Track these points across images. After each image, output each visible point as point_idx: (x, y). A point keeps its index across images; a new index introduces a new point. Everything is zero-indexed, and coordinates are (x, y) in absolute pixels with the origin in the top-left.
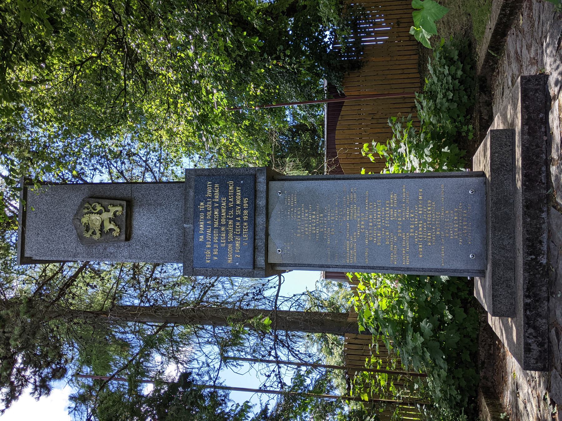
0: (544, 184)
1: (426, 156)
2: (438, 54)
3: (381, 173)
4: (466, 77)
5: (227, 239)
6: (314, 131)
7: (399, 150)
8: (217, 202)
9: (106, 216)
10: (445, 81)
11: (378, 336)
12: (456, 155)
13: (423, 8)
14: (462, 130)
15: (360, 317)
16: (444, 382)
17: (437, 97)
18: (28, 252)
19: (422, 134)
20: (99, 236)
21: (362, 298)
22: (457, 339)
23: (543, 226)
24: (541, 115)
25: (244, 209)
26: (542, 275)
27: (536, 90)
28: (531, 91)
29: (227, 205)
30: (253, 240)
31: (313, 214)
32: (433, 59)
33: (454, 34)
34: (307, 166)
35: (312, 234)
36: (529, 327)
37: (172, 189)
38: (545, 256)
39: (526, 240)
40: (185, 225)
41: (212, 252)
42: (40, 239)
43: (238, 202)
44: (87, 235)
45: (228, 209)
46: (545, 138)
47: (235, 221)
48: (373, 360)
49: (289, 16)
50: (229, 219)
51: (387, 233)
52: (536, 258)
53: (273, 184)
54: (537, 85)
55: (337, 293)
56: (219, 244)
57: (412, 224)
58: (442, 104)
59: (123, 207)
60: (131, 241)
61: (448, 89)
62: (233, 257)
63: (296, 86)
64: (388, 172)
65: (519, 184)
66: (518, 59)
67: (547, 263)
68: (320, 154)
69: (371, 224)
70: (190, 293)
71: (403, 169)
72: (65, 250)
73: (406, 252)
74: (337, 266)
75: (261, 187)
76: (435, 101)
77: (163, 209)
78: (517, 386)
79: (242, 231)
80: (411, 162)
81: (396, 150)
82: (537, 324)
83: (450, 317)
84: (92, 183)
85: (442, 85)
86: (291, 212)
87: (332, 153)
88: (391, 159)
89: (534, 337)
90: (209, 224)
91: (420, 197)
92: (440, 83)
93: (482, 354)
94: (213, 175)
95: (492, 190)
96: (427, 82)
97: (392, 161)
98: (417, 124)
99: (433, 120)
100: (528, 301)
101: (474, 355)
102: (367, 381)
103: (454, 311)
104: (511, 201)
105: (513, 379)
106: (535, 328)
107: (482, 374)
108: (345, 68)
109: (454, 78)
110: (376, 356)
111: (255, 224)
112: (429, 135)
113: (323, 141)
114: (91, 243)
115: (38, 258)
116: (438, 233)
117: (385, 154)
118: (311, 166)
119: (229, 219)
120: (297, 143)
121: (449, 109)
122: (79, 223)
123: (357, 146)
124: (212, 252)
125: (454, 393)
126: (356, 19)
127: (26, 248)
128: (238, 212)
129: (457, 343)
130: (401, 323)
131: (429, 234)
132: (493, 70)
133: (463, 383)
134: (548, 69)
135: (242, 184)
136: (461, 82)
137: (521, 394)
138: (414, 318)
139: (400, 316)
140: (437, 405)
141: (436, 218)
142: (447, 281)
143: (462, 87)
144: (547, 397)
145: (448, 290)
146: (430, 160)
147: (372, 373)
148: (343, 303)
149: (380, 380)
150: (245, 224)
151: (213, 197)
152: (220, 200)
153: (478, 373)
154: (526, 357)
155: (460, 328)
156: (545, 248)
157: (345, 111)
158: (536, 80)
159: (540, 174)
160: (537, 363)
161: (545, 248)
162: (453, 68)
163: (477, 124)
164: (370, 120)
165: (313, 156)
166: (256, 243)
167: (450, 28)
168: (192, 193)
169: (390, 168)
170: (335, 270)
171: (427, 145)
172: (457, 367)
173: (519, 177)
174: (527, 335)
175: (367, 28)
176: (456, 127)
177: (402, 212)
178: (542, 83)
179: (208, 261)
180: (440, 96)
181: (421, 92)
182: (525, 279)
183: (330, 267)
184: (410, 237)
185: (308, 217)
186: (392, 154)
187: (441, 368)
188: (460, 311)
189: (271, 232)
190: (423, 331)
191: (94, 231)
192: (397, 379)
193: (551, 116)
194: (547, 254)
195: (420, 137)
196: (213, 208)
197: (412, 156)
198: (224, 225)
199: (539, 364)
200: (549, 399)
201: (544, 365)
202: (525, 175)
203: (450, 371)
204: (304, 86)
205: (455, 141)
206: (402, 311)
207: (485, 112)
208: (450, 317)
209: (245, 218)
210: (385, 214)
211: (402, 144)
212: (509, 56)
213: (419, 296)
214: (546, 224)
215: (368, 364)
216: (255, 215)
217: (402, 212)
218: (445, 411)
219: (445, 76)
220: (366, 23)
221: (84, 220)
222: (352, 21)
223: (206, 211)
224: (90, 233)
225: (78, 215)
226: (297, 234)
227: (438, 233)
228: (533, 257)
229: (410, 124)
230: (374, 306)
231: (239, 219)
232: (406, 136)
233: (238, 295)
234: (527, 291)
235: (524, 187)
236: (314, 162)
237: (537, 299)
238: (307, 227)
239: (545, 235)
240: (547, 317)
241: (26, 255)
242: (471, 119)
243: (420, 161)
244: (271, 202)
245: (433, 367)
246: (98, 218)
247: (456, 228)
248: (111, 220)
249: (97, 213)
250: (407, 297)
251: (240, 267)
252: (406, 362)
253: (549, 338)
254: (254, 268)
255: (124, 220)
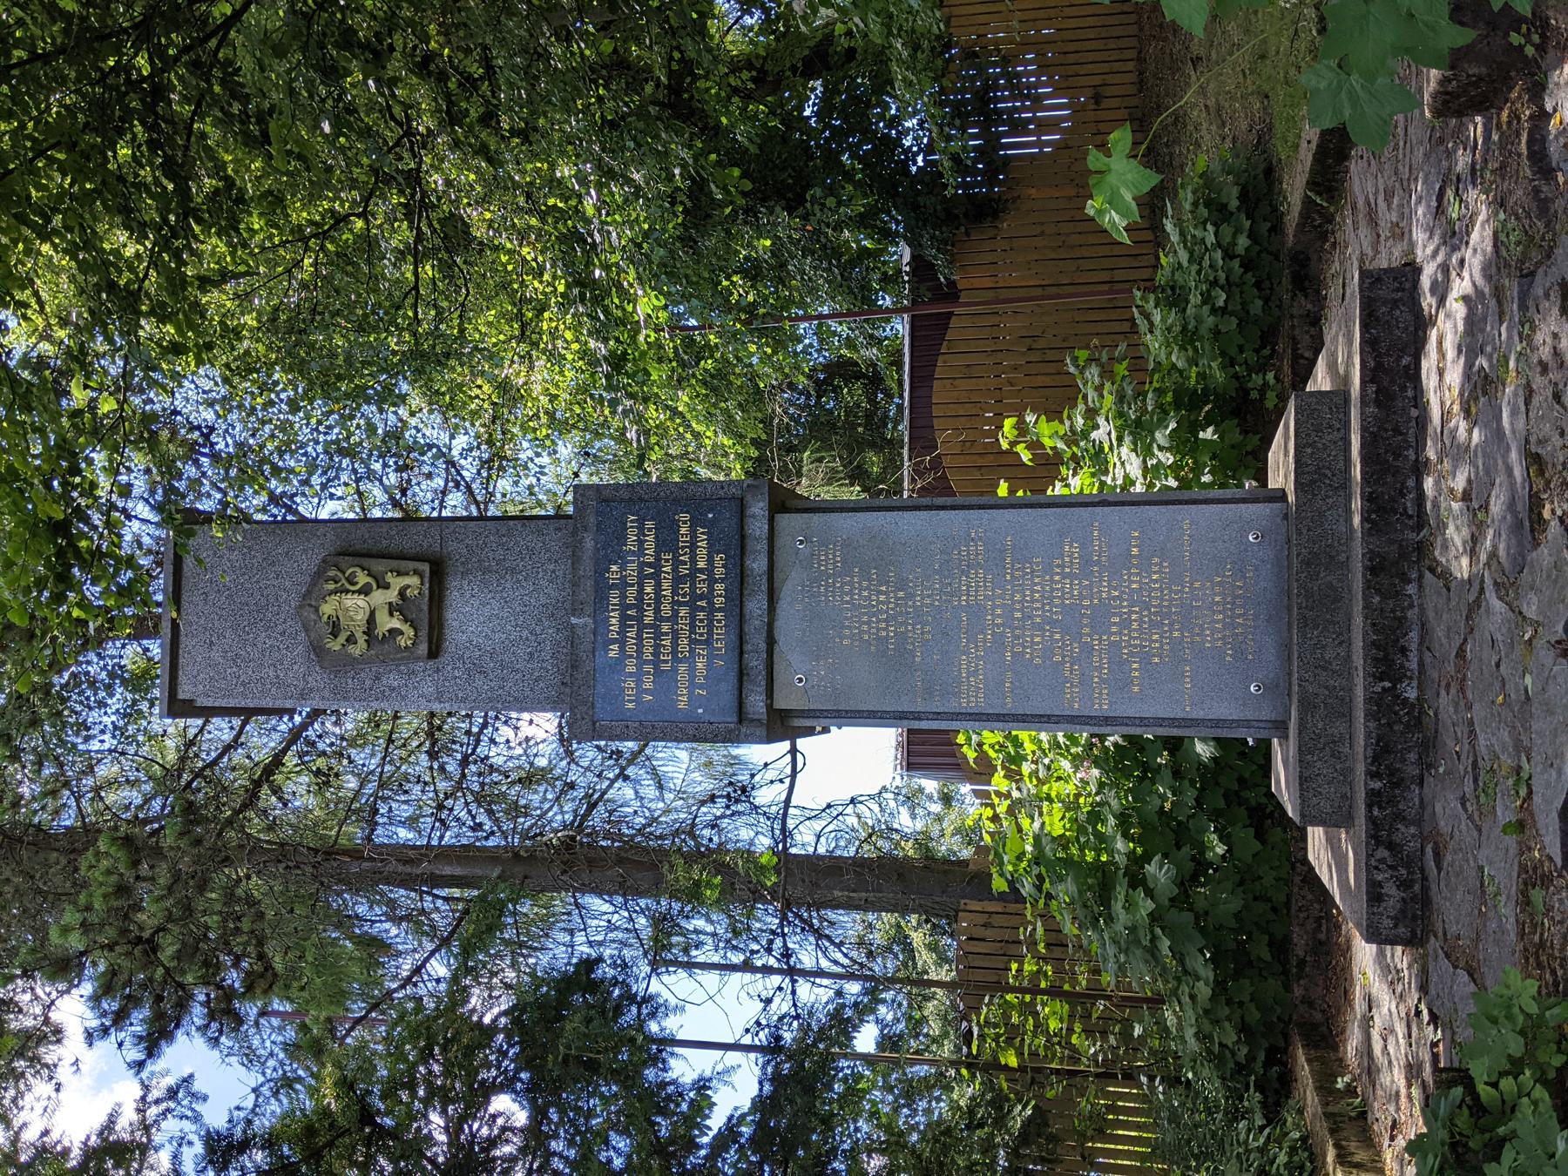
0: (1411, 517)
1: (1161, 448)
2: (1190, 195)
3: (1049, 492)
4: (1260, 252)
5: (674, 652)
6: (874, 381)
7: (1094, 435)
8: (650, 565)
9: (379, 598)
10: (1206, 263)
11: (1042, 902)
12: (1233, 447)
13: (1110, 170)
14: (1250, 385)
15: (997, 854)
16: (1206, 1012)
17: (1187, 302)
18: (186, 688)
19: (1150, 395)
20: (365, 646)
21: (1002, 809)
22: (1236, 904)
23: (1409, 614)
24: (1405, 361)
25: (716, 581)
26: (1407, 726)
27: (1395, 304)
28: (1385, 303)
29: (675, 570)
30: (737, 652)
31: (881, 593)
32: (1178, 208)
33: (1234, 140)
34: (857, 475)
35: (879, 638)
36: (1378, 843)
37: (540, 532)
38: (1415, 683)
39: (1370, 645)
40: (574, 620)
41: (639, 682)
42: (216, 655)
43: (701, 565)
44: (335, 645)
45: (677, 580)
46: (1414, 413)
47: (694, 609)
48: (1029, 967)
49: (810, 74)
50: (681, 604)
51: (1057, 636)
52: (1394, 687)
53: (784, 520)
54: (1398, 290)
55: (939, 819)
56: (656, 663)
57: (1115, 614)
58: (1199, 320)
59: (422, 577)
60: (441, 659)
61: (1214, 283)
62: (691, 694)
63: (830, 263)
64: (1066, 491)
65: (1357, 520)
66: (1373, 221)
67: (1418, 699)
68: (890, 442)
69: (1018, 615)
70: (550, 809)
71: (1103, 483)
72: (279, 683)
73: (1102, 681)
74: (938, 716)
75: (757, 526)
76: (1184, 310)
77: (518, 581)
78: (1370, 1003)
79: (710, 633)
80: (1123, 463)
81: (1085, 435)
82: (1397, 838)
83: (1220, 849)
84: (316, 521)
85: (1199, 272)
86: (827, 585)
87: (923, 438)
88: (1074, 457)
89: (1390, 867)
90: (631, 618)
91: (1135, 551)
92: (1195, 267)
93: (1300, 943)
94: (641, 499)
95: (1299, 533)
96: (1163, 260)
97: (1077, 462)
98: (1138, 364)
99: (1177, 359)
100: (1376, 785)
101: (1281, 947)
102: (1015, 1019)
103: (1229, 836)
104: (1342, 558)
105: (1363, 987)
106: (1391, 846)
107: (1298, 992)
108: (957, 217)
109: (1229, 255)
110: (1039, 958)
111: (742, 615)
112: (1169, 398)
113: (900, 407)
114: (340, 665)
115: (209, 703)
116: (1176, 634)
117: (1061, 445)
118: (867, 474)
119: (681, 604)
120: (830, 412)
121: (1216, 332)
122: (313, 617)
123: (988, 421)
124: (639, 682)
125: (1231, 1038)
126: (986, 88)
127: (182, 678)
128: (702, 588)
129: (1237, 916)
130: (1097, 866)
131: (1155, 637)
132: (1324, 237)
133: (1254, 1016)
134: (1420, 254)
135: (710, 521)
136: (1247, 265)
137: (1376, 1018)
138: (1131, 855)
139: (1098, 852)
140: (1190, 1075)
141: (1171, 600)
142: (1214, 759)
143: (1250, 278)
144: (1423, 1007)
145: (1217, 784)
146: (1168, 459)
147: (1028, 998)
148: (955, 848)
149: (1047, 1018)
150: (719, 615)
151: (641, 551)
152: (658, 559)
153: (1287, 988)
154: (1371, 914)
155: (1244, 878)
156: (1413, 665)
157: (954, 332)
158: (1395, 279)
159: (1404, 496)
160: (1396, 926)
161: (1413, 665)
162: (1226, 230)
163: (1287, 369)
164: (1023, 354)
165: (873, 445)
166: (745, 662)
167: (1223, 124)
168: (589, 544)
169: (1071, 481)
170: (934, 725)
171: (1162, 423)
172: (1236, 976)
173: (1357, 504)
174: (1373, 863)
175: (1015, 109)
176: (1236, 377)
177: (1090, 586)
178: (1407, 286)
179: (631, 706)
180: (1196, 299)
181: (1149, 287)
182: (1368, 736)
183: (920, 719)
184: (1111, 644)
185: (869, 598)
186: (1078, 445)
187: (1198, 979)
188: (1244, 834)
189: (780, 636)
190: (1151, 886)
191: (352, 635)
192: (1090, 1016)
193: (1424, 364)
194: (1419, 678)
195: (1144, 400)
196: (642, 578)
197: (1125, 450)
198: (668, 619)
199: (1402, 930)
200: (1425, 1012)
201: (1413, 932)
202: (1368, 498)
203: (1219, 986)
204: (849, 261)
205: (1236, 413)
206: (1101, 838)
207: (1305, 340)
208: (1220, 849)
209: (719, 601)
210: (1052, 590)
211: (1101, 421)
212: (1354, 208)
213: (1144, 802)
214: (1416, 610)
215: (1016, 977)
216: (741, 594)
217: (1090, 586)
218: (1212, 1087)
219: (1207, 249)
220: (1013, 98)
221: (327, 609)
222: (975, 93)
223: (623, 584)
224: (342, 639)
225: (311, 597)
226: (841, 638)
227: (1176, 634)
228: (1387, 684)
229: (1121, 369)
230: (1030, 826)
231: (703, 603)
232: (1109, 400)
233: (674, 816)
234: (1372, 764)
235: (1367, 526)
236: (874, 462)
237: (1396, 781)
238: (868, 623)
239: (1414, 635)
240: (1418, 822)
241: (181, 696)
242: (1271, 356)
243: (1144, 461)
244: (779, 565)
245: (1178, 979)
246: (361, 603)
247: (1218, 622)
248: (392, 609)
249: (359, 592)
250: (1114, 803)
251: (707, 718)
252: (1111, 965)
253: (1422, 870)
254: (740, 721)
255: (425, 608)
